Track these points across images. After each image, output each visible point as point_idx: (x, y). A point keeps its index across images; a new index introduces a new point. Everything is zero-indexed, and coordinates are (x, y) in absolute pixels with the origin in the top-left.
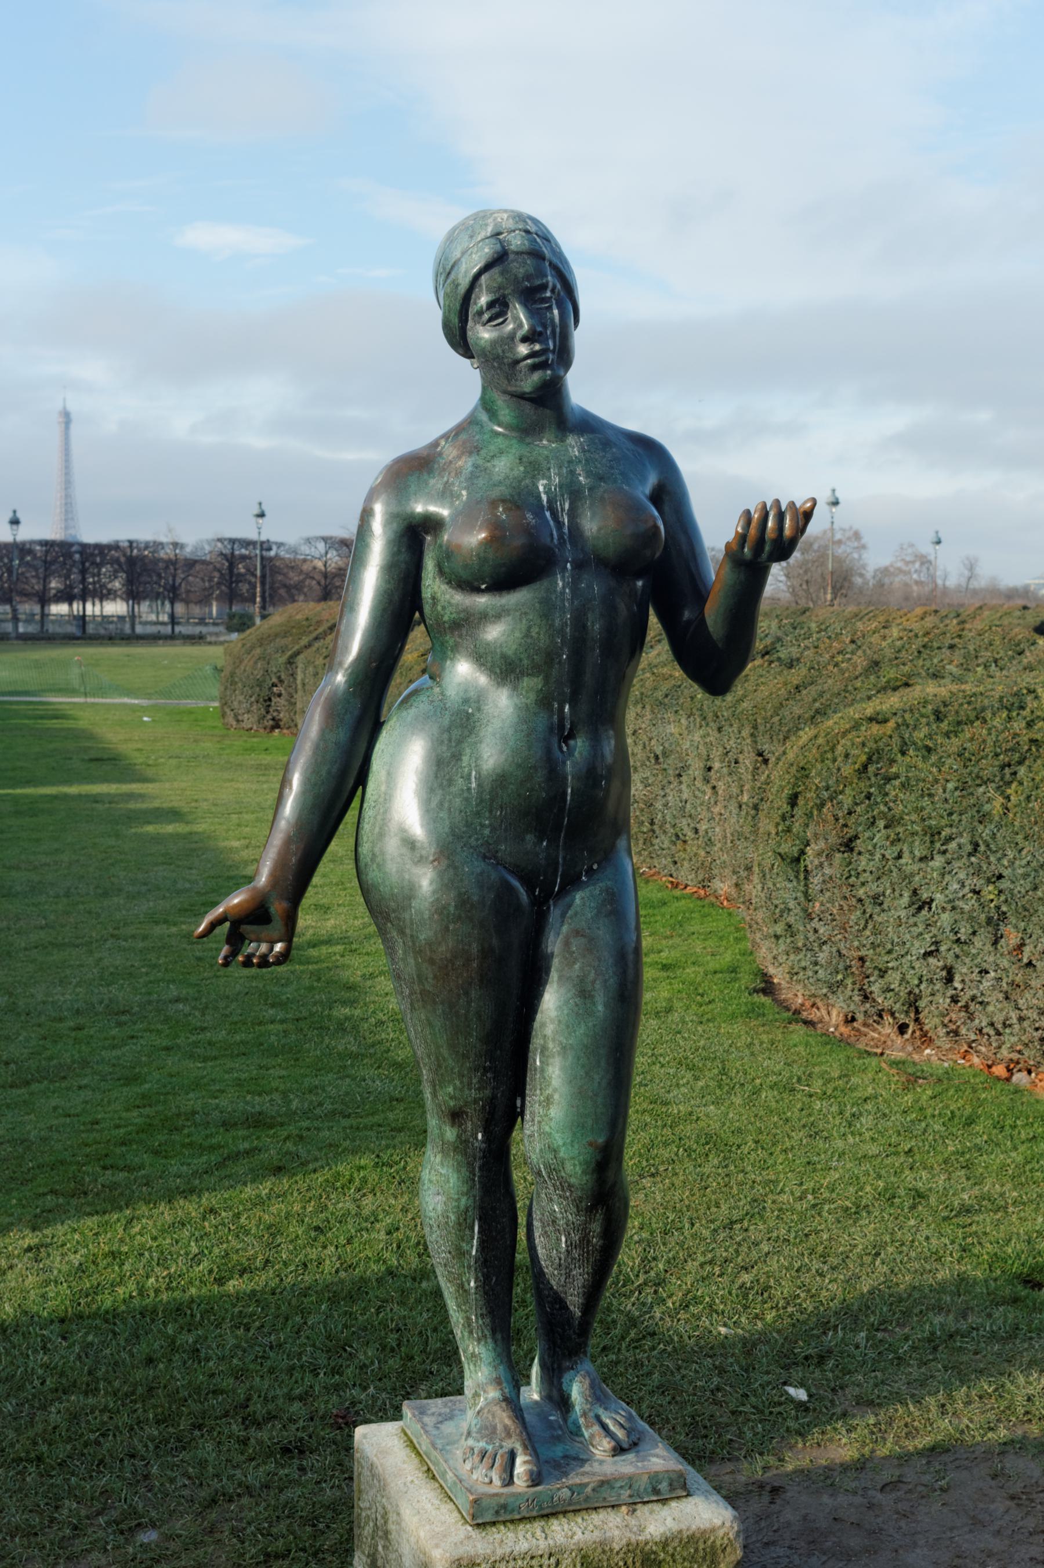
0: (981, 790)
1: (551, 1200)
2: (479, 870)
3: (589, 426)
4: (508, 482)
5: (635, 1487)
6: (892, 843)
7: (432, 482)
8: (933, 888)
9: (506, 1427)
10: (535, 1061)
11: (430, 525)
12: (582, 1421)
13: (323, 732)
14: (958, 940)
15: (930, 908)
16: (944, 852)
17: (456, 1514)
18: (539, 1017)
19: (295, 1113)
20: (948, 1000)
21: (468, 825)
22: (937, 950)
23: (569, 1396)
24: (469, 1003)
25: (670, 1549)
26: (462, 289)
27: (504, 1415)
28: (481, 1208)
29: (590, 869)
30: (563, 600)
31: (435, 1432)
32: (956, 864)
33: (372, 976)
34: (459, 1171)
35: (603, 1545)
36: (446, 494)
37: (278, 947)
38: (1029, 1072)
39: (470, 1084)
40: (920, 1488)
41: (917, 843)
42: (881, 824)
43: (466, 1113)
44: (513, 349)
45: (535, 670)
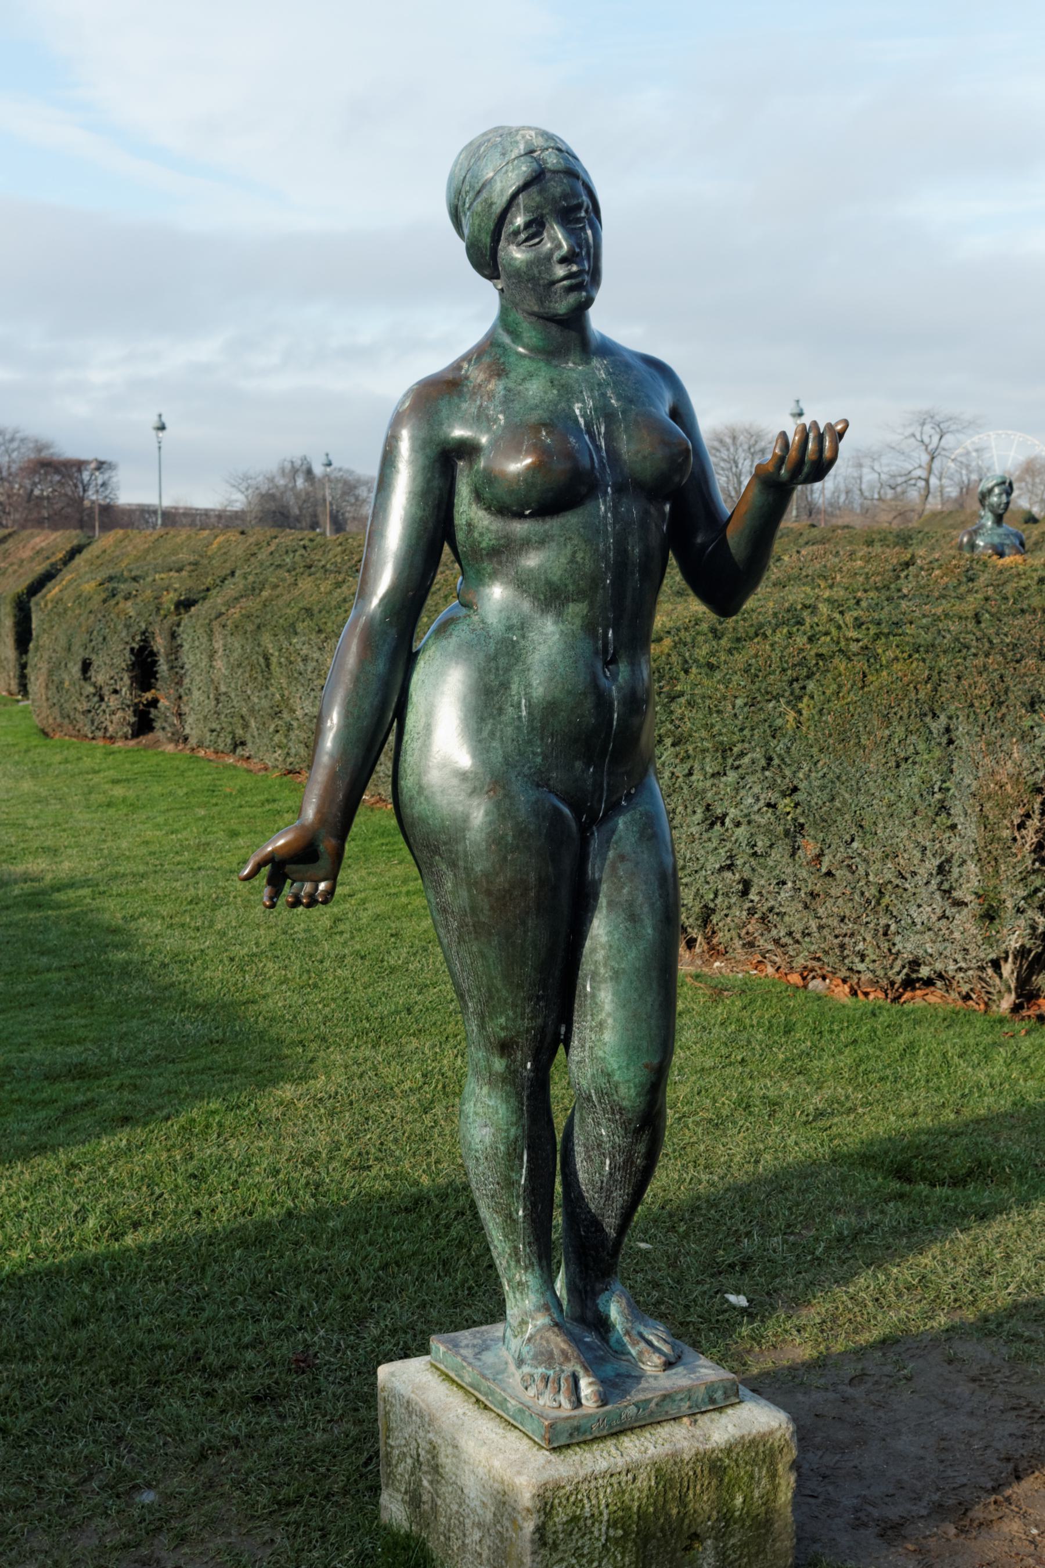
0: (771, 705)
1: (599, 1124)
2: (533, 799)
3: (607, 349)
5: (694, 1398)
6: (682, 760)
7: (464, 406)
8: (726, 803)
9: (563, 1352)
10: (585, 987)
11: (467, 450)
12: (626, 1339)
14: (755, 854)
15: (723, 824)
16: (737, 768)
17: (526, 1440)
18: (588, 944)
19: (118, 1061)
20: (745, 913)
21: (521, 754)
22: (732, 864)
23: (608, 1317)
25: (734, 1455)
26: (497, 209)
27: (559, 1339)
28: (530, 1137)
29: (629, 793)
30: (606, 525)
31: (478, 1363)
32: (750, 779)
34: (508, 1102)
35: (675, 1457)
36: (481, 419)
37: (322, 886)
38: (824, 978)
39: (523, 1014)
40: (885, 1379)
41: (708, 760)
42: (668, 741)
43: (517, 1044)
44: (549, 270)
45: (581, 595)
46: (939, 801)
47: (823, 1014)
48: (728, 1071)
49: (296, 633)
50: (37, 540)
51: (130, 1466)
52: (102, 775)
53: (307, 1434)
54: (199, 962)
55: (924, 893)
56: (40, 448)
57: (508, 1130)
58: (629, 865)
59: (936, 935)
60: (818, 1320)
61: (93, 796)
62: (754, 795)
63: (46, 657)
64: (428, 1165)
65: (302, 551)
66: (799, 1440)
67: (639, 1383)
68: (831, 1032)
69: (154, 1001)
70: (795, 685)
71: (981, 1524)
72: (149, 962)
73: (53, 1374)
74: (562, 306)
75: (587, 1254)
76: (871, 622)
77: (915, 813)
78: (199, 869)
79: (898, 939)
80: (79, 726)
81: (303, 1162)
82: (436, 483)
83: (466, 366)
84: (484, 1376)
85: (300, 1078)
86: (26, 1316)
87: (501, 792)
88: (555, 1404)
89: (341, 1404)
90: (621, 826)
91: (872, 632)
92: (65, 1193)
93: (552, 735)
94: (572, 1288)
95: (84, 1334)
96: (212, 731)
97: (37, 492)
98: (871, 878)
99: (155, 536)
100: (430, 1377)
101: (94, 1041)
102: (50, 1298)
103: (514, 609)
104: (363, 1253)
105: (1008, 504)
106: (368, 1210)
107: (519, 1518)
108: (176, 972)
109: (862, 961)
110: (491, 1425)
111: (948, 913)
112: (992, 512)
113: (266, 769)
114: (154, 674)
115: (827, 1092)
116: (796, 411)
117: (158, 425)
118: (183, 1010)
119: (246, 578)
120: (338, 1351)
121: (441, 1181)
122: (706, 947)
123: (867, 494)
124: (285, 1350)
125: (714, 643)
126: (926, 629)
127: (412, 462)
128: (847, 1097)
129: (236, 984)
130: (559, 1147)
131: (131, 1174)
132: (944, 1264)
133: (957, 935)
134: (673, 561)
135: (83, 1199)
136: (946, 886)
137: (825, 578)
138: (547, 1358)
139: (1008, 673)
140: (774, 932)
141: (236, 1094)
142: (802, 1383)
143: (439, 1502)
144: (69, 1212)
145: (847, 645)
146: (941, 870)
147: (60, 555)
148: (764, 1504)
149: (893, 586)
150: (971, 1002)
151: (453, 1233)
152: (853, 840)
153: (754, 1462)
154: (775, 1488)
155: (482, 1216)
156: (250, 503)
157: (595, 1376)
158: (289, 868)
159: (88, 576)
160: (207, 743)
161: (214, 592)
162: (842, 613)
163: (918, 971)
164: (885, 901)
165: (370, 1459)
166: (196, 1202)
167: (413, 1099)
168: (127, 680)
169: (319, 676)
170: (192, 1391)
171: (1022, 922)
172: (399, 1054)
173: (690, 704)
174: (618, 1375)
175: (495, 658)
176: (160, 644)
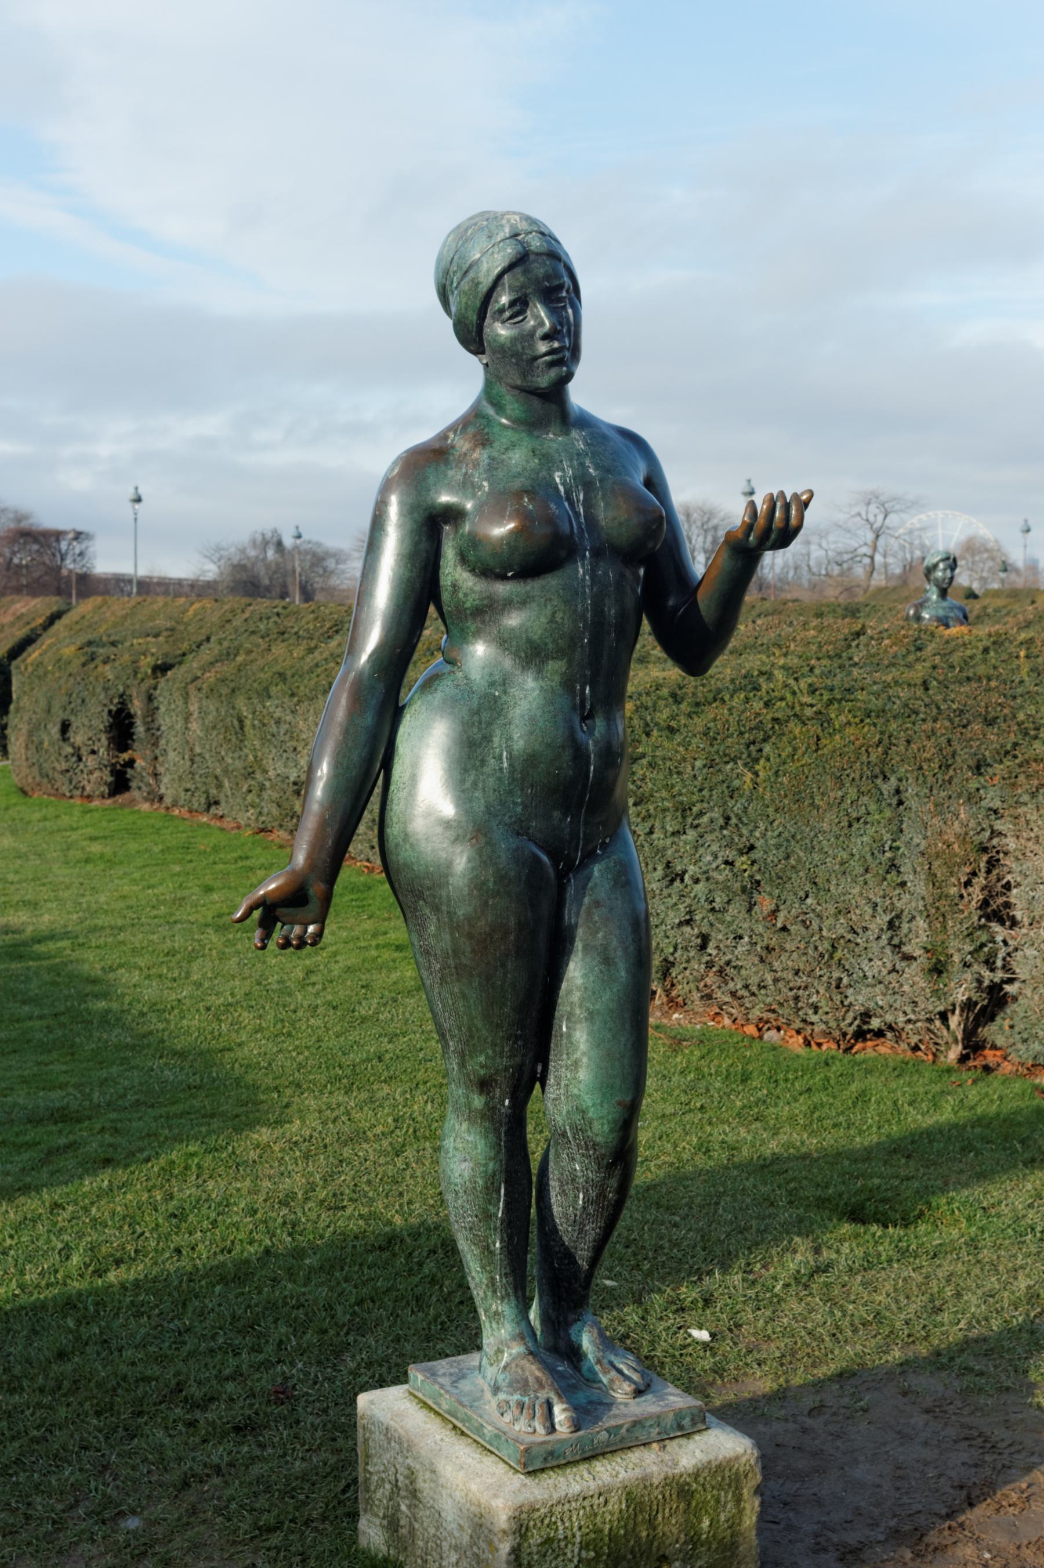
1: (573, 1159)
2: (514, 846)
3: (585, 422)
4: (527, 474)
5: (663, 1424)
6: (643, 819)
7: (451, 473)
8: (686, 861)
9: (537, 1379)
10: (561, 1027)
11: (453, 515)
12: (597, 1368)
13: (351, 714)
14: (713, 910)
15: (682, 880)
16: (696, 827)
17: (502, 1465)
18: (564, 986)
19: (99, 1106)
20: (703, 966)
21: (502, 803)
22: (691, 920)
23: (580, 1346)
24: (505, 974)
25: (701, 1480)
26: (484, 288)
27: (533, 1367)
29: (604, 842)
30: (584, 587)
31: (455, 1391)
32: (708, 837)
33: (112, 969)
34: (486, 1137)
35: (645, 1481)
36: (466, 485)
37: (311, 929)
38: (779, 1029)
40: (843, 1411)
43: (496, 1081)
44: (532, 346)
45: (559, 653)
46: (889, 859)
47: (778, 1063)
48: (688, 1117)
49: (269, 697)
50: (18, 606)
51: (115, 1494)
52: (80, 832)
53: (287, 1462)
54: (176, 1011)
55: (875, 947)
56: (19, 518)
57: (486, 1165)
58: (604, 910)
59: (887, 988)
60: (778, 1354)
61: (71, 853)
62: (714, 851)
63: (26, 718)
64: (401, 1205)
65: (275, 618)
66: (764, 1468)
67: (610, 1410)
68: (786, 1080)
69: (133, 1048)
70: (752, 748)
71: (936, 1549)
72: (128, 1011)
73: (39, 1405)
74: (544, 380)
75: (560, 1286)
76: (825, 688)
77: (867, 871)
78: (175, 922)
79: (850, 992)
80: (57, 785)
81: (280, 1202)
82: (423, 546)
83: (452, 436)
84: (461, 1403)
85: (276, 1122)
86: (12, 1349)
87: (482, 840)
88: (530, 1430)
89: (319, 1433)
90: (596, 873)
91: (825, 698)
92: (49, 1231)
93: (532, 786)
94: (546, 1318)
95: (69, 1367)
96: (187, 790)
97: (16, 561)
98: (824, 933)
99: (133, 603)
100: (408, 1405)
101: (76, 1086)
102: (34, 1331)
103: (497, 665)
104: (339, 1290)
105: (952, 578)
106: (343, 1248)
107: (496, 1539)
108: (154, 1020)
109: (816, 1013)
110: (468, 1450)
111: (898, 967)
112: (937, 586)
113: (239, 827)
114: (130, 736)
115: (783, 1138)
116: (747, 490)
117: (134, 497)
118: (161, 1057)
119: (221, 644)
120: (315, 1383)
121: (413, 1221)
122: (665, 999)
123: (814, 570)
124: (264, 1382)
125: (674, 707)
126: (877, 695)
127: (400, 526)
128: (803, 1143)
129: (212, 1032)
130: (534, 1179)
131: (113, 1214)
132: (897, 1301)
133: (906, 988)
134: (646, 626)
135: (66, 1238)
136: (896, 941)
137: (780, 647)
138: (522, 1385)
139: (955, 737)
140: (731, 985)
141: (214, 1137)
142: (763, 1415)
143: (417, 1526)
144: (53, 1249)
145: (802, 710)
146: (891, 925)
147: (40, 621)
148: (730, 1527)
149: (844, 655)
150: (919, 1053)
151: (426, 1270)
152: (807, 896)
153: (720, 1487)
154: (741, 1512)
155: (460, 1247)
156: (222, 573)
157: (568, 1402)
158: (280, 911)
159: (67, 641)
160: (181, 803)
161: (190, 657)
162: (796, 679)
163: (868, 1023)
164: (838, 955)
165: (348, 1486)
166: (176, 1240)
167: (385, 1143)
168: (104, 741)
169: (292, 738)
170: (174, 1421)
171: (968, 976)
172: (371, 1100)
173: (652, 765)
174: (591, 1402)
175: (478, 712)
176: (137, 707)
